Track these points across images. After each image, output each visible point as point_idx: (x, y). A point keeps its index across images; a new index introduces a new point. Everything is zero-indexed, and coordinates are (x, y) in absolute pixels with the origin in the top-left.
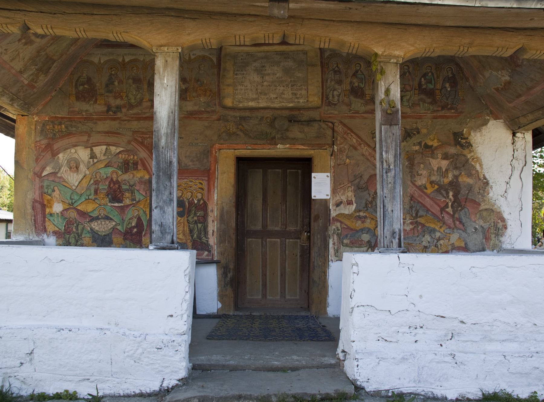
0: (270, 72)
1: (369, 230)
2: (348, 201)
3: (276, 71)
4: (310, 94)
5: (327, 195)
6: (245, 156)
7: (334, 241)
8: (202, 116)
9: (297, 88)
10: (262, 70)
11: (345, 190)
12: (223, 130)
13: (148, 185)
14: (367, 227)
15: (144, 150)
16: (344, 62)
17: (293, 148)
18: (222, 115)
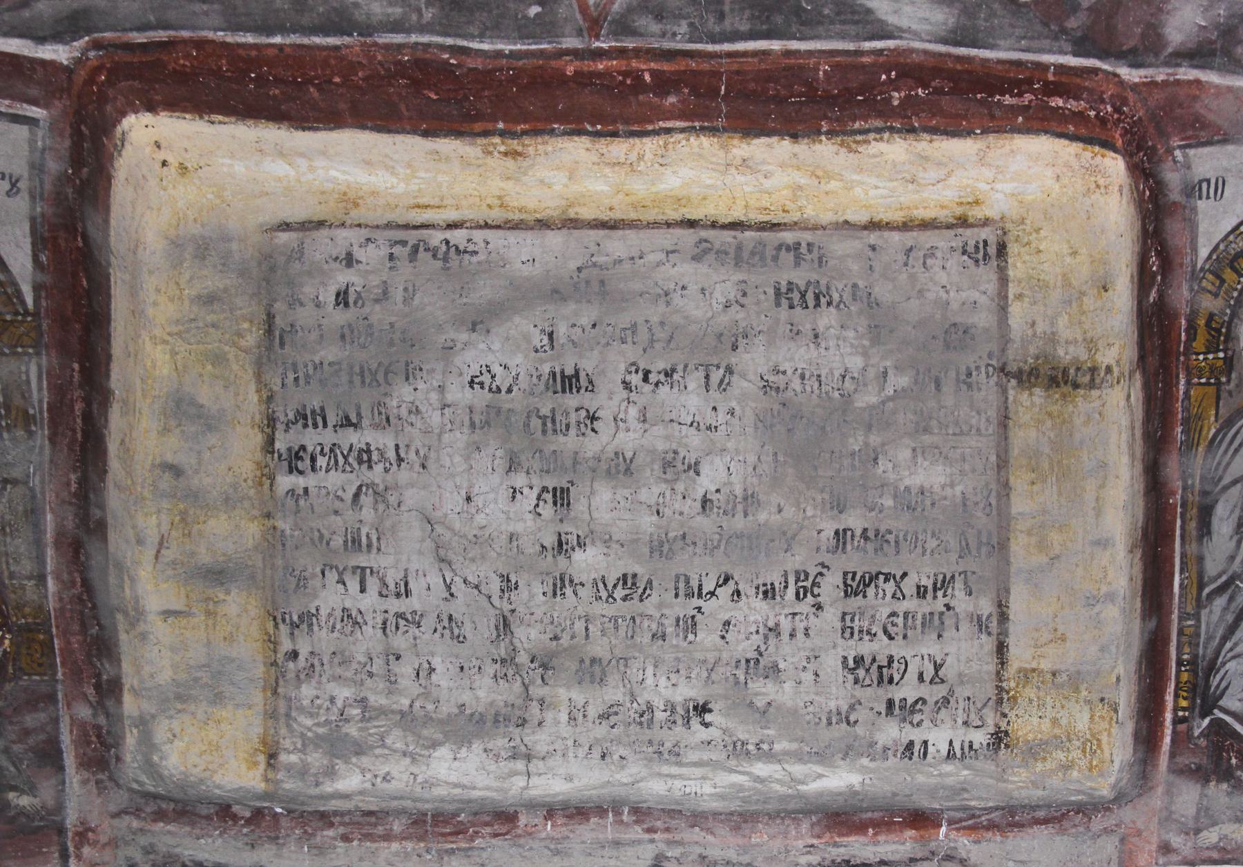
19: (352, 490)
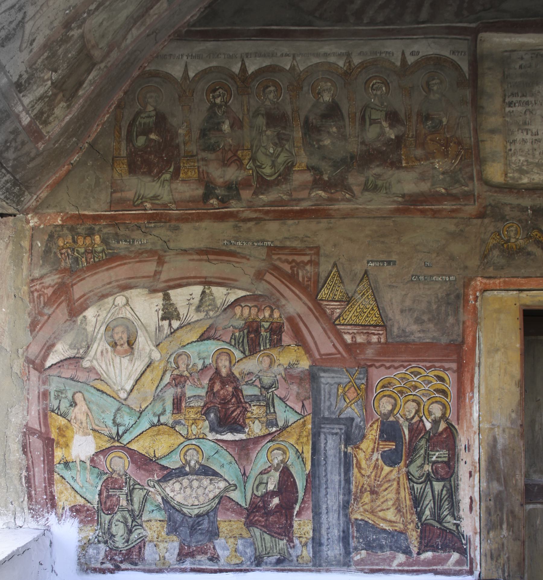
8: (440, 207)
12: (492, 242)
13: (307, 386)
18: (490, 205)
19: (524, 111)
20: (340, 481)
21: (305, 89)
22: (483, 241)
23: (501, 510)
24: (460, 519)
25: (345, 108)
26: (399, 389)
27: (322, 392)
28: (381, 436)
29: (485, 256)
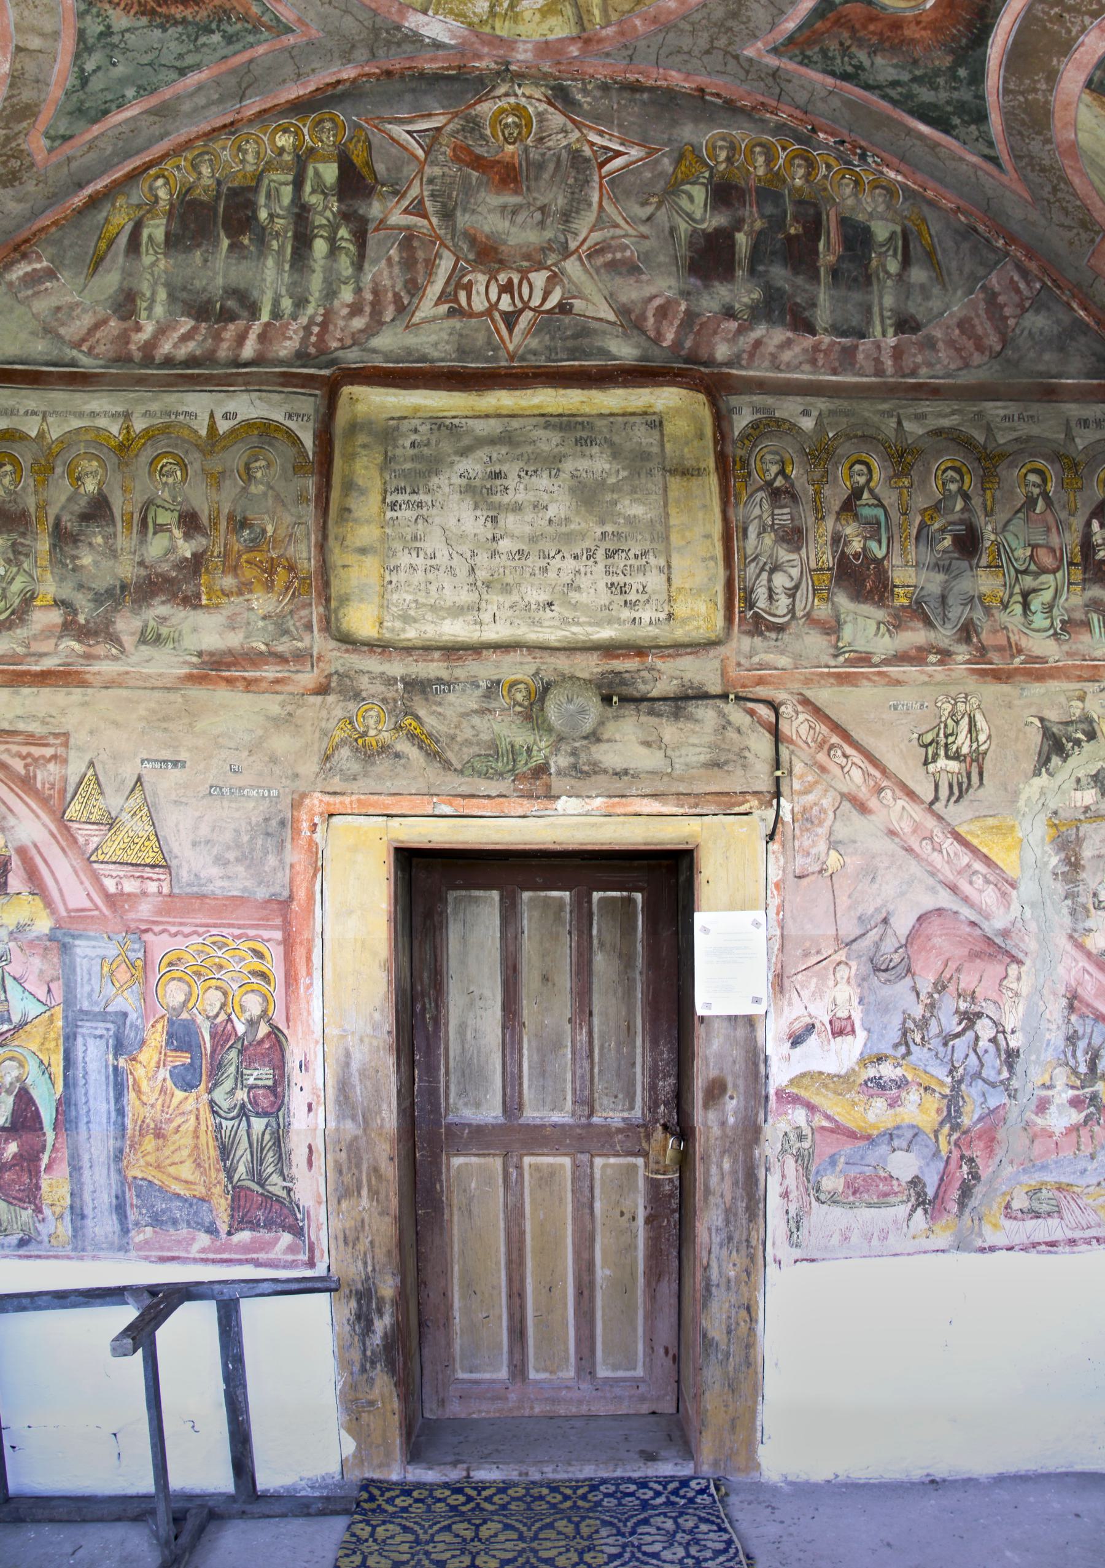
0: (520, 497)
1: (916, 1135)
2: (837, 1025)
3: (546, 497)
4: (680, 590)
5: (757, 1001)
6: (429, 846)
7: (786, 1182)
8: (258, 674)
9: (629, 563)
10: (491, 491)
11: (823, 978)
12: (339, 735)
13: (55, 960)
14: (907, 1121)
15: (33, 811)
16: (807, 454)
17: (619, 811)
18: (336, 672)
20: (109, 1113)
21: (59, 470)
22: (325, 733)
23: (358, 1166)
24: (292, 1180)
25: (117, 504)
26: (195, 968)
27: (78, 970)
28: (169, 1043)
29: (327, 758)
